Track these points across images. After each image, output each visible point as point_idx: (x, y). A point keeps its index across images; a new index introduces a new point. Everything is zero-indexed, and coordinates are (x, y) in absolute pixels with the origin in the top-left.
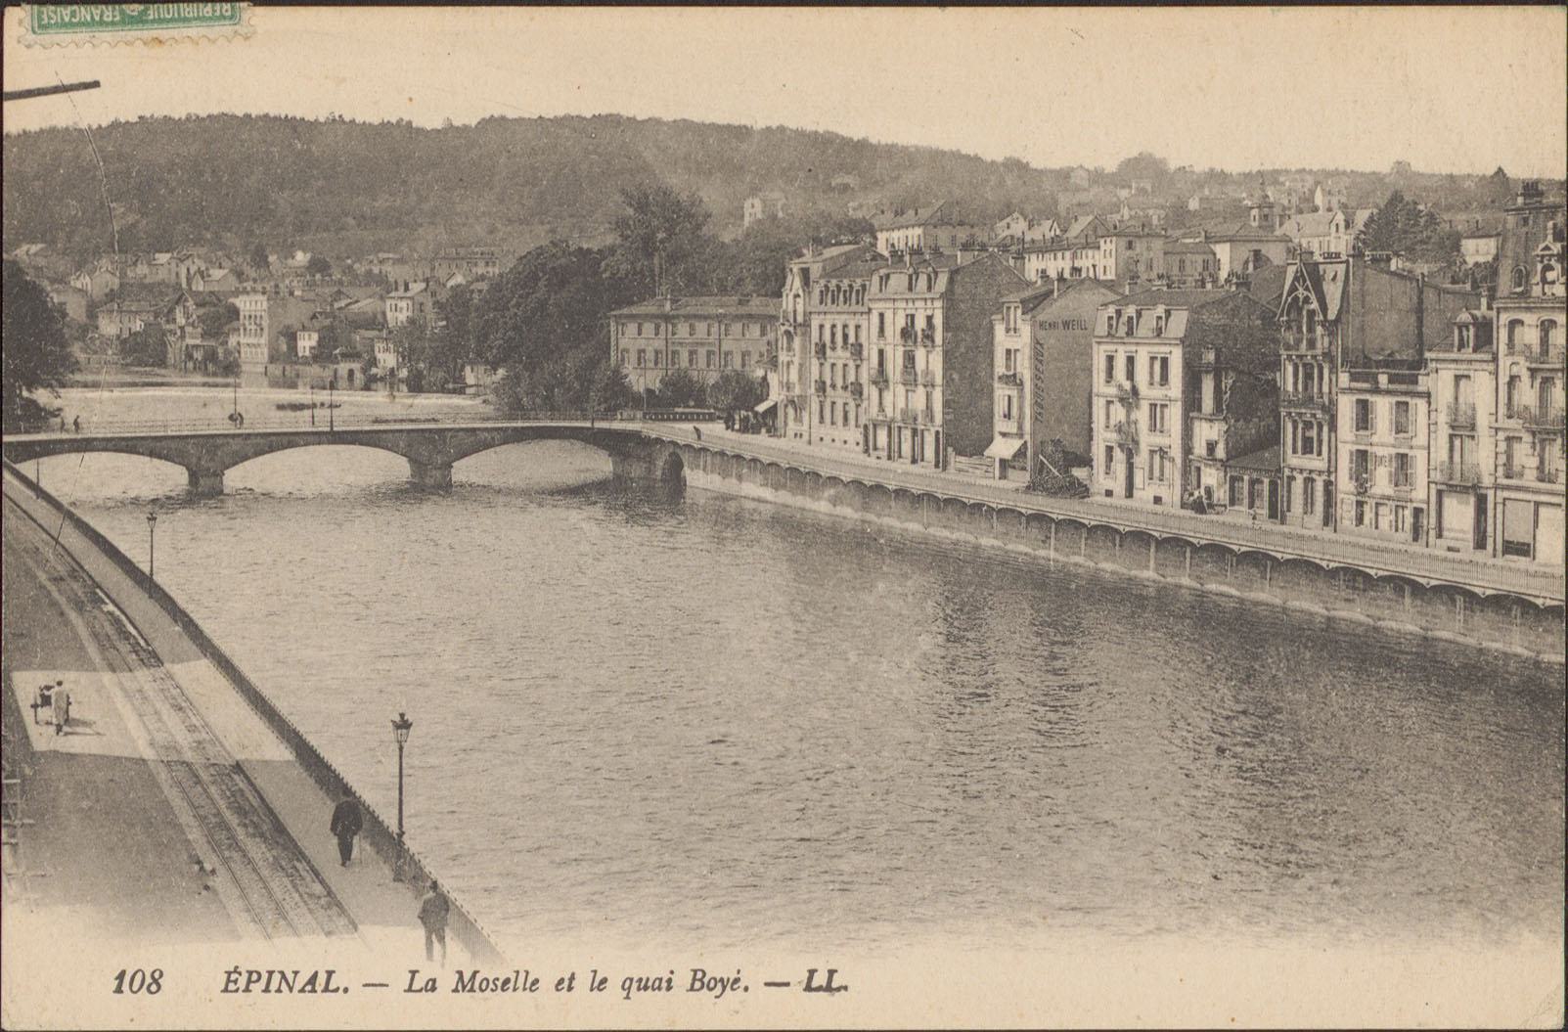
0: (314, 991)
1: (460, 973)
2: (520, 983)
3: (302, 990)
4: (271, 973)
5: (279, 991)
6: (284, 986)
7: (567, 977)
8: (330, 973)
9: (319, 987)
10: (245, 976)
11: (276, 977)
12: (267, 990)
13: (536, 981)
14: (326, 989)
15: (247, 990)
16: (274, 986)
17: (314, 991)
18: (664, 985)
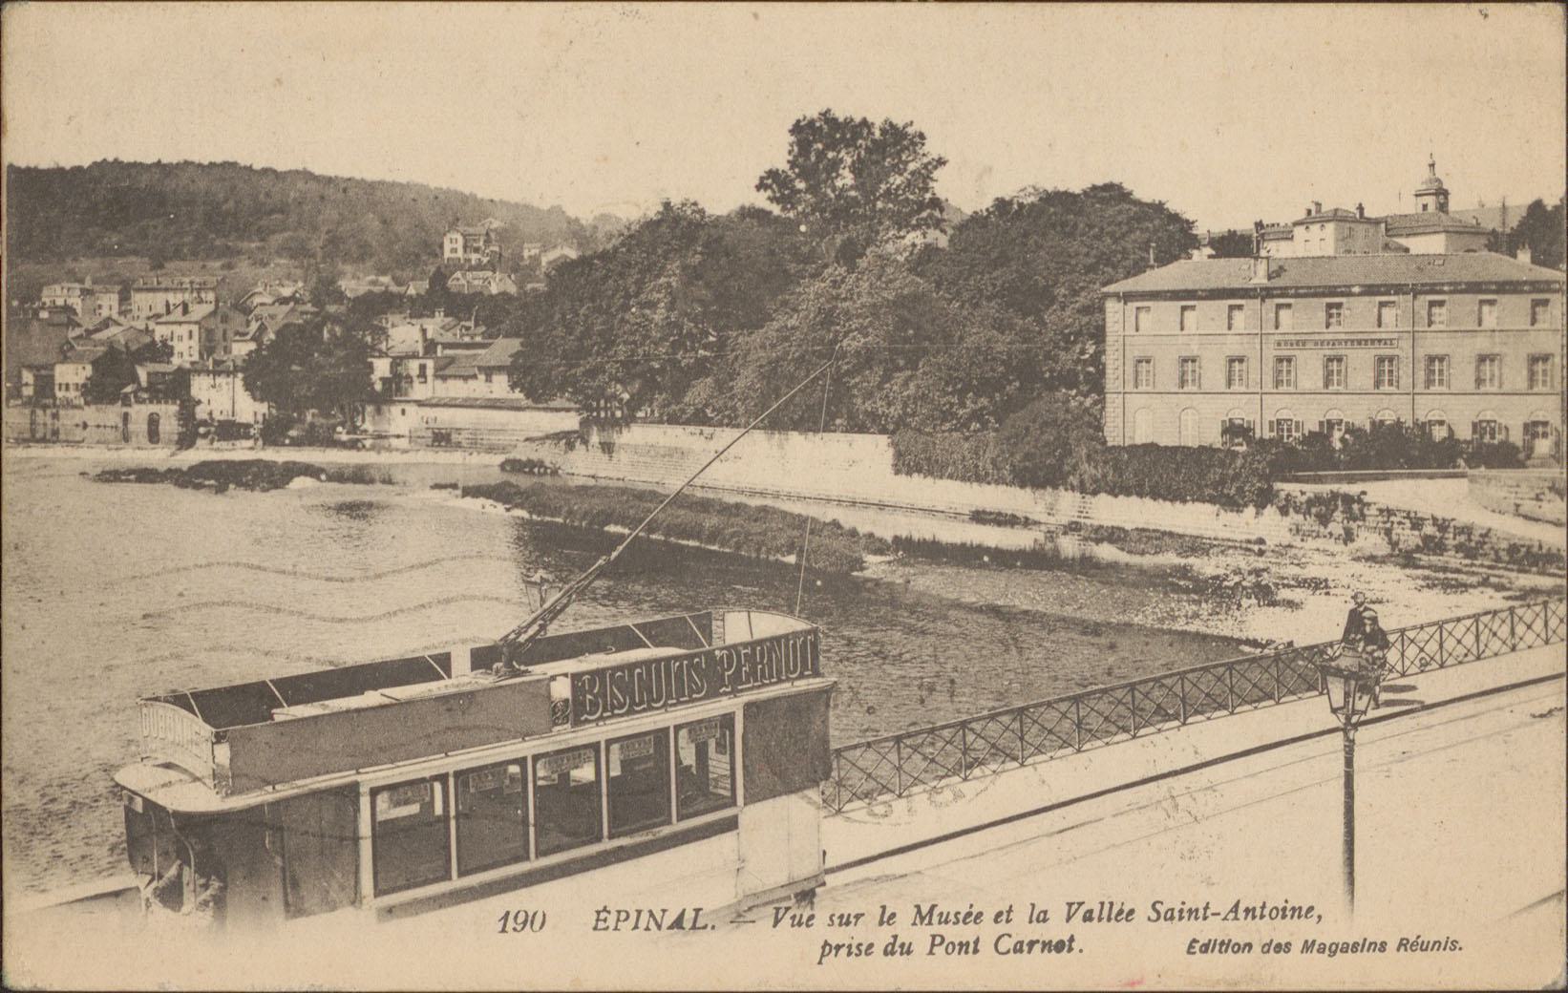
0: (1236, 918)
1: (918, 907)
3: (670, 928)
4: (639, 912)
5: (647, 929)
7: (1066, 938)
9: (687, 924)
11: (645, 916)
12: (636, 927)
13: (893, 915)
14: (694, 927)
16: (642, 924)
17: (1236, 918)
18: (1176, 914)
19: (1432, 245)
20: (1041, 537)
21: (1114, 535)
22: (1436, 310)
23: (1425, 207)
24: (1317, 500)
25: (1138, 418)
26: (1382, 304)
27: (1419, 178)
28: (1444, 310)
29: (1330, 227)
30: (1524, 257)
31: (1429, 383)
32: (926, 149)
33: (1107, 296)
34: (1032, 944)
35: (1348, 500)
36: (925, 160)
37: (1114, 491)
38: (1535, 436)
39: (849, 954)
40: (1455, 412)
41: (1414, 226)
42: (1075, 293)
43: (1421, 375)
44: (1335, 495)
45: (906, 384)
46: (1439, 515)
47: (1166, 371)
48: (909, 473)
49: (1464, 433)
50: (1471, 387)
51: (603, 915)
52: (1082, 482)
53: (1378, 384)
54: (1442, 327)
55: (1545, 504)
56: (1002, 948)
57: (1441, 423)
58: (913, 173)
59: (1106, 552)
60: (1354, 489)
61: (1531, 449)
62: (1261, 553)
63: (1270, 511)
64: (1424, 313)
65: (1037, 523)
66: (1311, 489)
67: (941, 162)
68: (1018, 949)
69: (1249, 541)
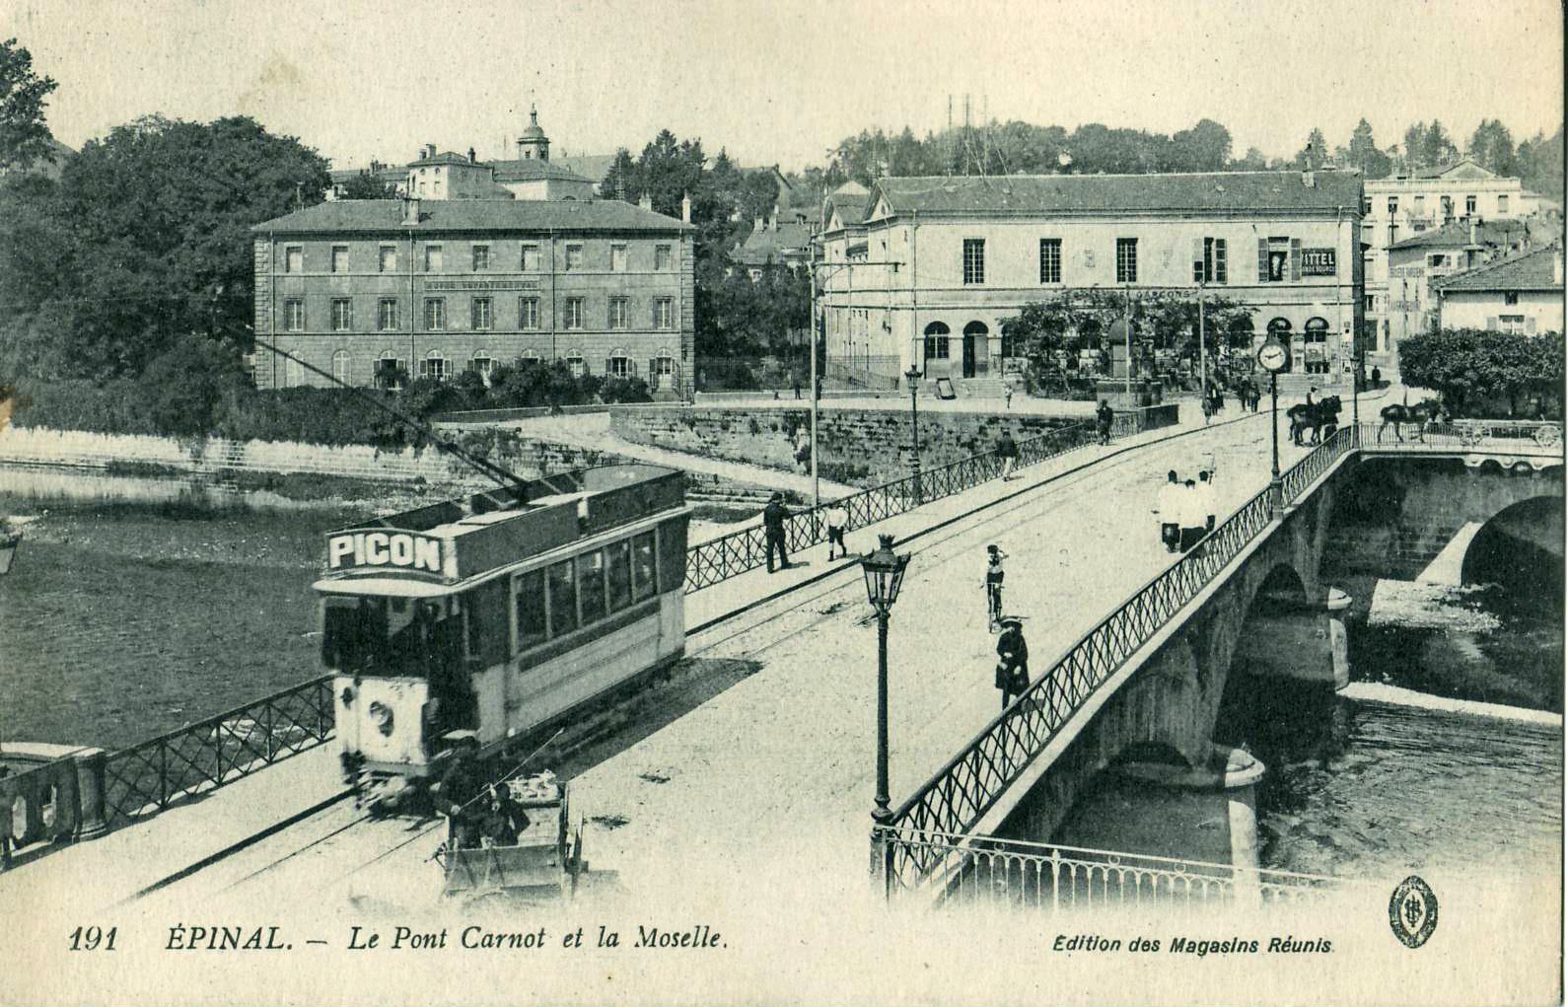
3: (246, 947)
6: (228, 943)
9: (264, 942)
12: (211, 947)
14: (270, 946)
16: (218, 943)
19: (535, 191)
20: (188, 487)
21: (271, 482)
22: (573, 255)
23: (528, 153)
24: (473, 438)
25: (290, 362)
26: (525, 247)
27: (520, 126)
28: (579, 255)
29: (444, 170)
30: (646, 205)
31: (568, 324)
32: (32, 70)
33: (256, 235)
35: (505, 437)
36: (31, 81)
37: (268, 438)
38: (660, 371)
40: (592, 354)
41: (520, 172)
42: (206, 231)
43: (561, 315)
44: (491, 433)
45: (25, 328)
46: (589, 448)
47: (317, 312)
48: (31, 425)
49: (599, 371)
50: (604, 327)
52: (233, 429)
53: (522, 325)
54: (579, 271)
55: (676, 434)
56: (469, 941)
57: (579, 360)
58: (17, 95)
59: (259, 499)
60: (508, 426)
61: (657, 382)
62: (422, 492)
63: (429, 451)
64: (563, 256)
65: (185, 473)
66: (469, 427)
67: (49, 85)
68: (488, 942)
69: (409, 481)
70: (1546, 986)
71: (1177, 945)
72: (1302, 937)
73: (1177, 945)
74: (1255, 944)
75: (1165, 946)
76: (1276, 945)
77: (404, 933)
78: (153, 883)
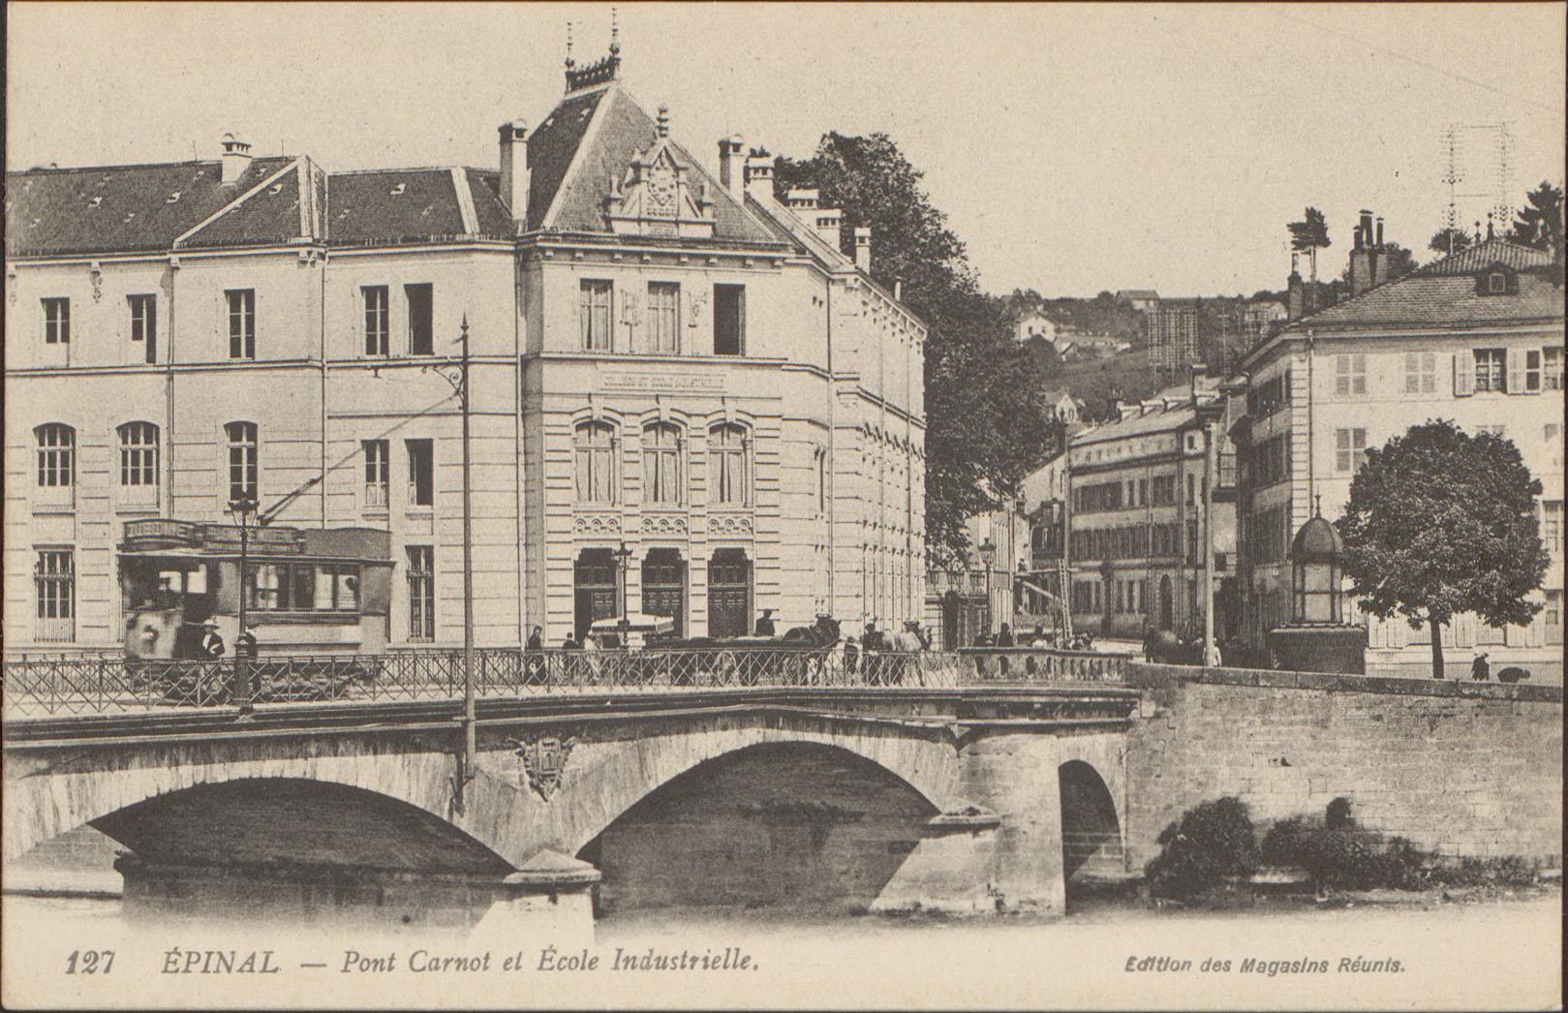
2: (731, 962)
3: (241, 970)
4: (210, 954)
6: (223, 968)
7: (515, 956)
8: (268, 955)
9: (258, 965)
10: (185, 957)
11: (215, 958)
12: (205, 971)
14: (264, 970)
15: (187, 971)
16: (212, 967)
34: (447, 962)
39: (705, 967)
51: (173, 957)
56: (417, 965)
68: (435, 965)
70: (1549, 989)
71: (1324, 967)
72: (1370, 957)
73: (1324, 967)
74: (1325, 964)
75: (1236, 966)
76: (1345, 964)
77: (353, 957)
78: (22, 887)
